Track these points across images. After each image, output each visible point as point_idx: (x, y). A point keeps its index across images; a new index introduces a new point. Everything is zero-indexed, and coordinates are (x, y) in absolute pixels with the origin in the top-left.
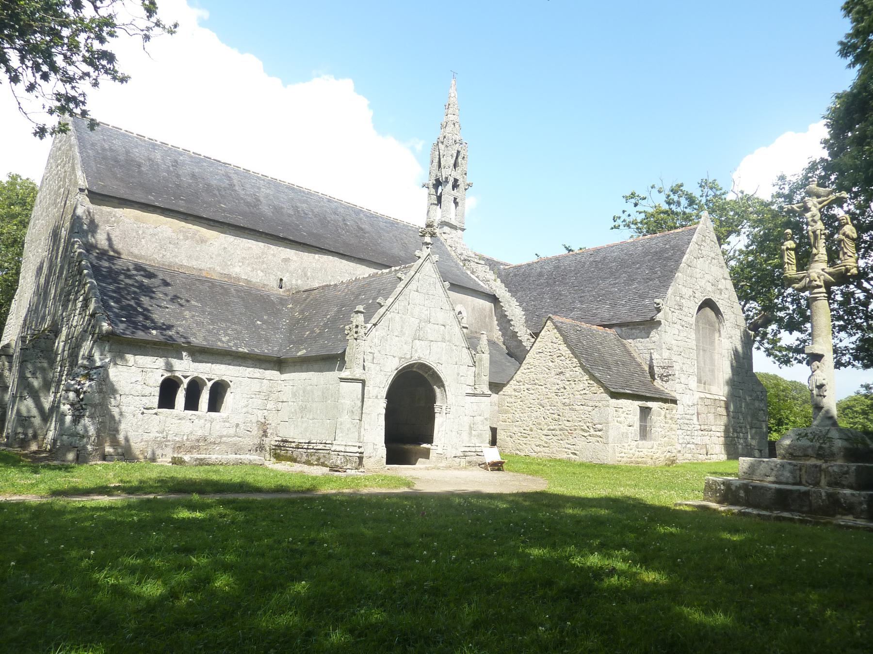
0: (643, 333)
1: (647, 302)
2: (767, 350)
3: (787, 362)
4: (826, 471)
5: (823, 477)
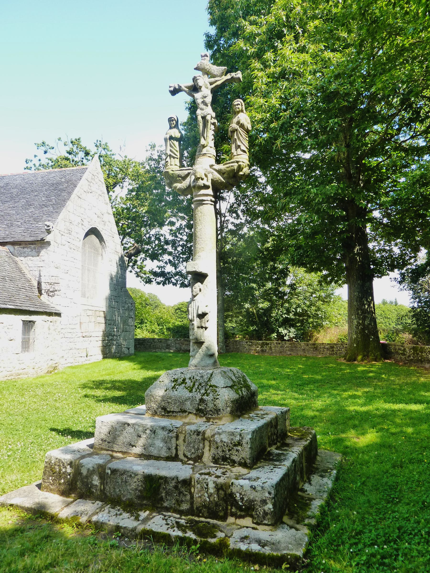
0: (34, 253)
1: (40, 224)
2: (137, 273)
3: (149, 281)
5: (207, 448)
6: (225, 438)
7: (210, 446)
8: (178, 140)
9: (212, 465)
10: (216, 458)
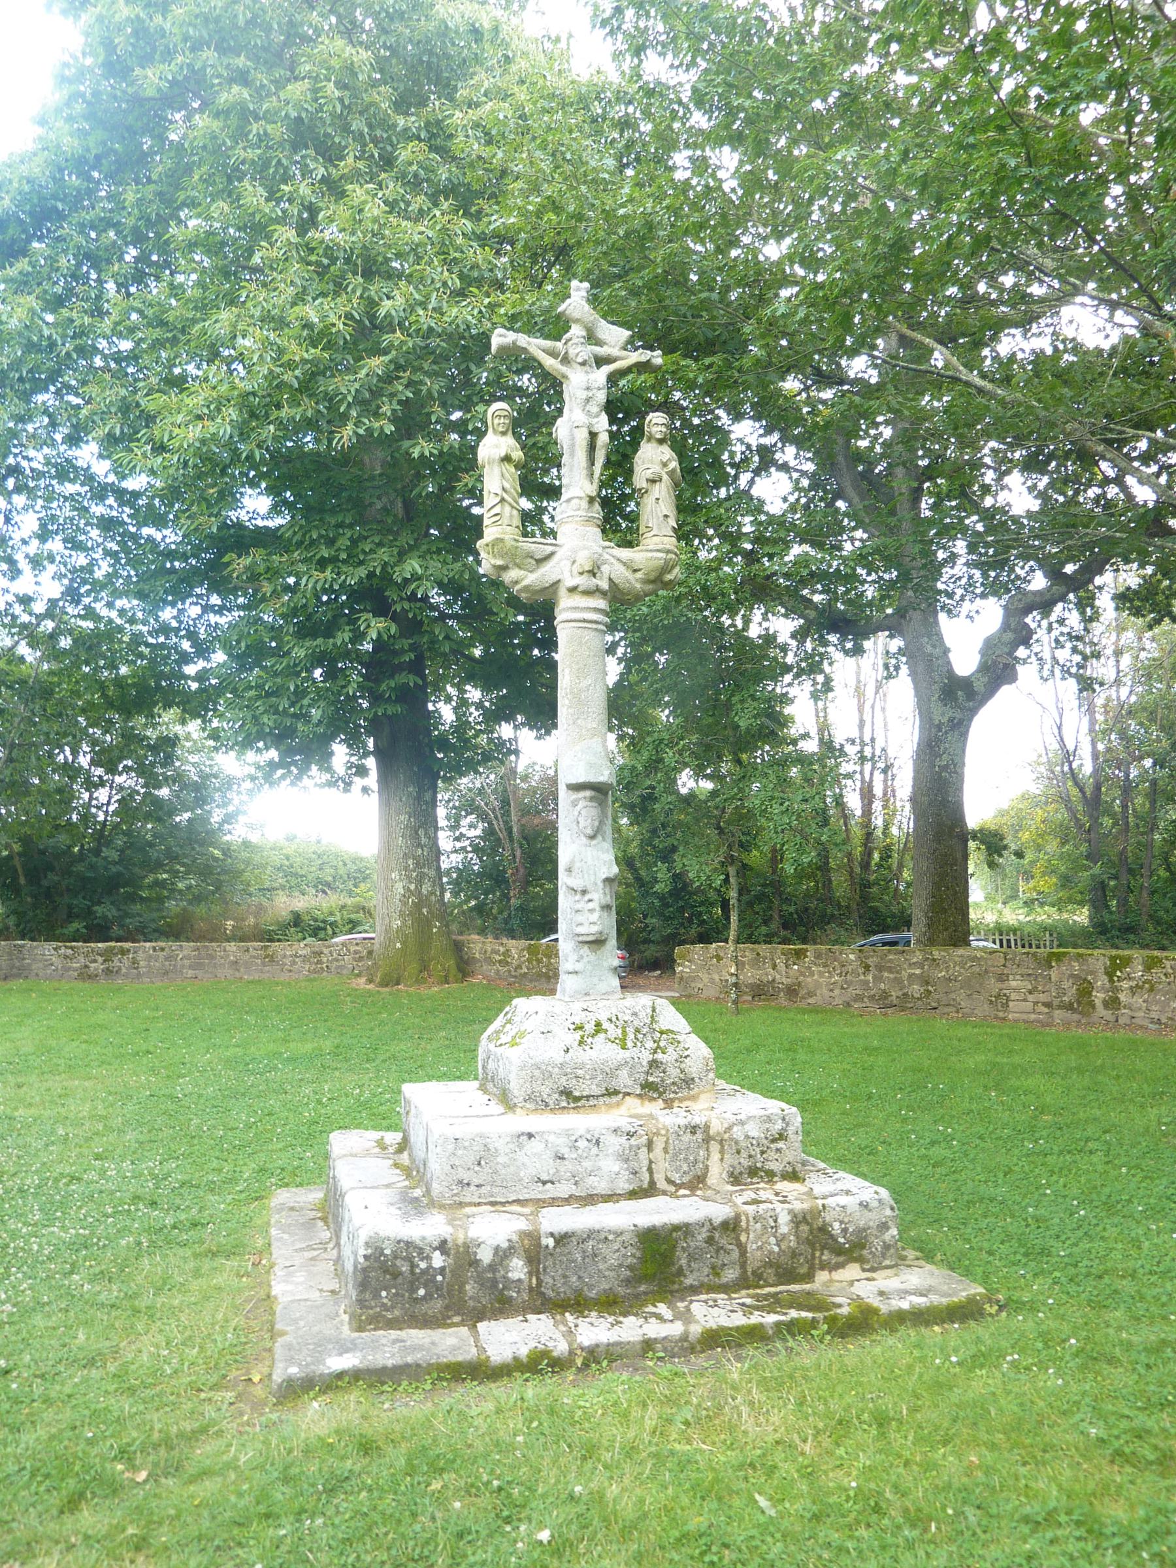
5: (715, 1156)
6: (754, 1130)
7: (722, 1152)
9: (730, 1188)
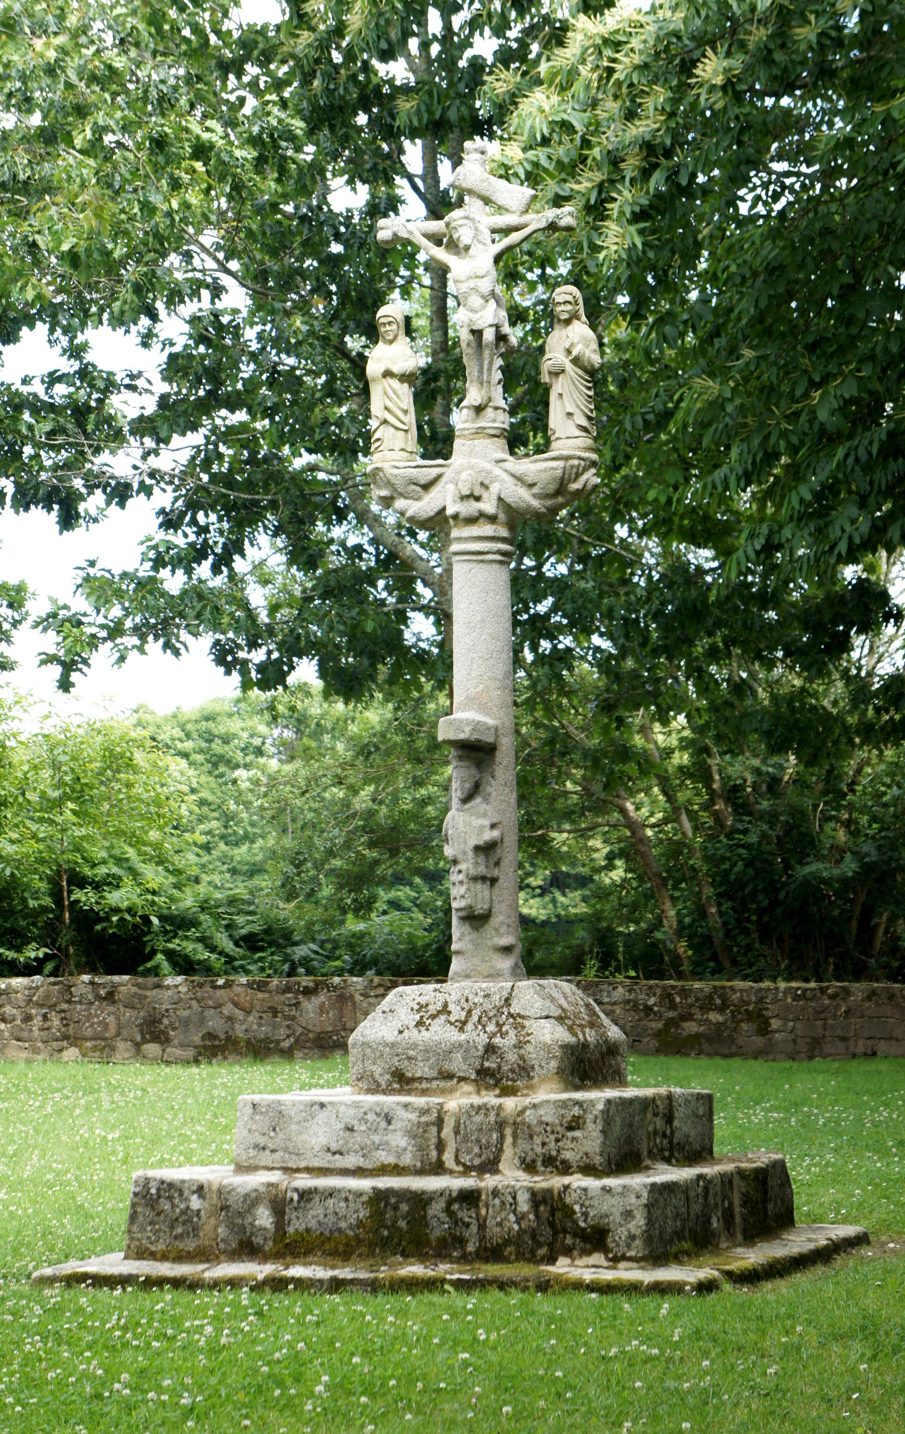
4: (519, 1127)
7: (515, 1136)
8: (405, 378)
10: (528, 1160)
